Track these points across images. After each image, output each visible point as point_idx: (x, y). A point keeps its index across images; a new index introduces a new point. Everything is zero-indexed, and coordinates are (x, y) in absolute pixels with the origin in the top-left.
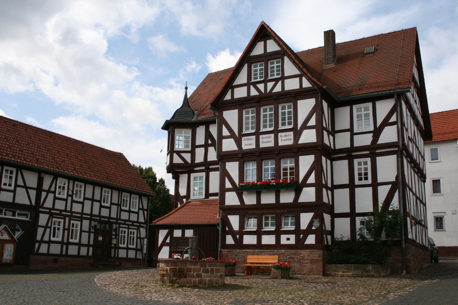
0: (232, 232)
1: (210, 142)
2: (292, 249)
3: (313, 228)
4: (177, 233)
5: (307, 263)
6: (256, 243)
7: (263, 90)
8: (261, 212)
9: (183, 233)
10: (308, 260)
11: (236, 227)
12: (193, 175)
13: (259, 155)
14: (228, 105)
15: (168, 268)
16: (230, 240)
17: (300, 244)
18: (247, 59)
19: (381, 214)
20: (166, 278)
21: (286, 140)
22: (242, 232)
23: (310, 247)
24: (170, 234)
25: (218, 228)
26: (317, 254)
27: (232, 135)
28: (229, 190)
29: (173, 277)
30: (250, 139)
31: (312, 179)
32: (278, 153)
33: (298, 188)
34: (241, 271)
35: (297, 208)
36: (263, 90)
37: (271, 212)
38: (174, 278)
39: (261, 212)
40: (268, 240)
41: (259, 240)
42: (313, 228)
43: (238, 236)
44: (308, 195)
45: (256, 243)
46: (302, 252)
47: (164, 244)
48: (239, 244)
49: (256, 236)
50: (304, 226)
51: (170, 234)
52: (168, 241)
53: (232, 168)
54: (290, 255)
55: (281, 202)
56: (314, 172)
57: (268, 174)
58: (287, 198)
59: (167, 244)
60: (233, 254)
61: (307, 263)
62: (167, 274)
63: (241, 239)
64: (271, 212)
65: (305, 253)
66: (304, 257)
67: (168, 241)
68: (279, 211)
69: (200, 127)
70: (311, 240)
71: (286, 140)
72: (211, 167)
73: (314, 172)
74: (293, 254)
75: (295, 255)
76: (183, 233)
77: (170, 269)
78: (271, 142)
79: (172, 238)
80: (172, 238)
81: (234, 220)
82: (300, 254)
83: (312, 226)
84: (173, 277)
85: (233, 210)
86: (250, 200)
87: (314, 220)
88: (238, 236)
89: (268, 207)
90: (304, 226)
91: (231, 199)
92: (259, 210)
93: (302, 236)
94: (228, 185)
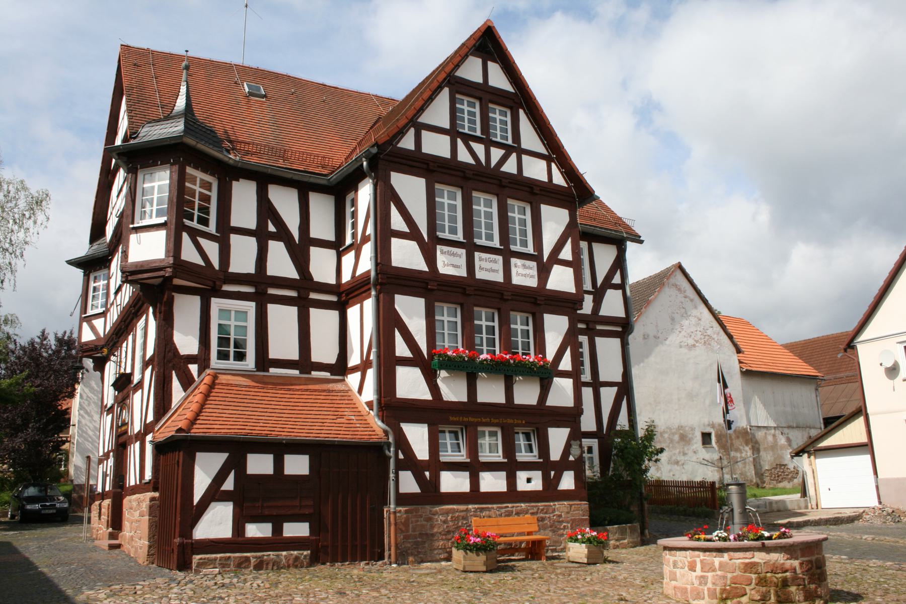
0: (409, 462)
1: (272, 228)
2: (538, 502)
3: (571, 458)
4: (259, 464)
5: (565, 528)
6: (468, 490)
7: (494, 162)
8: (476, 420)
9: (279, 464)
10: (568, 522)
11: (422, 452)
12: (216, 304)
13: (466, 293)
14: (397, 160)
15: (796, 563)
16: (408, 483)
17: (550, 492)
18: (447, 79)
19: (605, 435)
20: (793, 589)
21: (525, 275)
22: (436, 465)
23: (566, 495)
24: (236, 463)
25: (387, 452)
26: (581, 508)
27: (413, 234)
28: (404, 362)
29: (809, 584)
30: (454, 255)
31: (566, 364)
32: (504, 298)
33: (545, 375)
34: (442, 556)
35: (541, 418)
36: (494, 162)
37: (455, 419)
38: (813, 586)
39: (476, 420)
40: (493, 482)
41: (475, 482)
42: (571, 458)
43: (427, 474)
44: (562, 392)
45: (468, 490)
46: (557, 504)
47: (214, 494)
48: (431, 493)
49: (467, 474)
50: (555, 454)
51: (236, 463)
52: (229, 485)
53: (411, 310)
54: (537, 513)
55: (516, 402)
56: (569, 349)
57: (482, 338)
58: (526, 394)
59: (225, 497)
60: (421, 516)
61: (565, 528)
62: (795, 578)
63: (436, 481)
64: (455, 419)
65: (561, 507)
66: (560, 516)
67: (229, 485)
68: (507, 417)
69: (360, 185)
70: (567, 482)
71: (525, 275)
72: (272, 291)
73: (569, 349)
74: (542, 510)
75: (546, 513)
76: (279, 464)
77: (801, 564)
78: (497, 271)
79: (243, 478)
80: (243, 478)
81: (417, 436)
82: (554, 510)
83: (569, 454)
84: (809, 584)
85: (413, 411)
86: (453, 390)
87: (572, 442)
88: (427, 474)
89: (491, 409)
90: (555, 454)
91: (411, 384)
92: (467, 418)
93: (553, 473)
94: (402, 349)
